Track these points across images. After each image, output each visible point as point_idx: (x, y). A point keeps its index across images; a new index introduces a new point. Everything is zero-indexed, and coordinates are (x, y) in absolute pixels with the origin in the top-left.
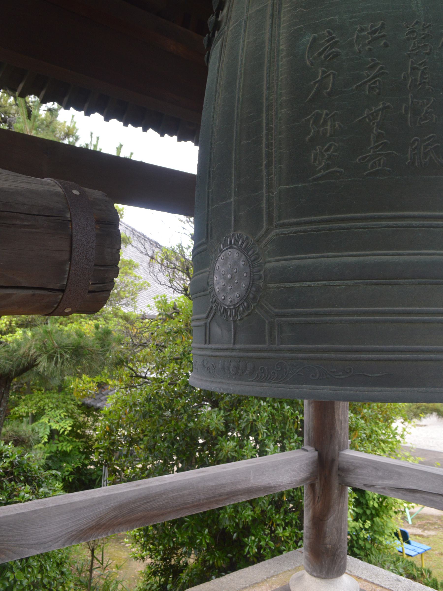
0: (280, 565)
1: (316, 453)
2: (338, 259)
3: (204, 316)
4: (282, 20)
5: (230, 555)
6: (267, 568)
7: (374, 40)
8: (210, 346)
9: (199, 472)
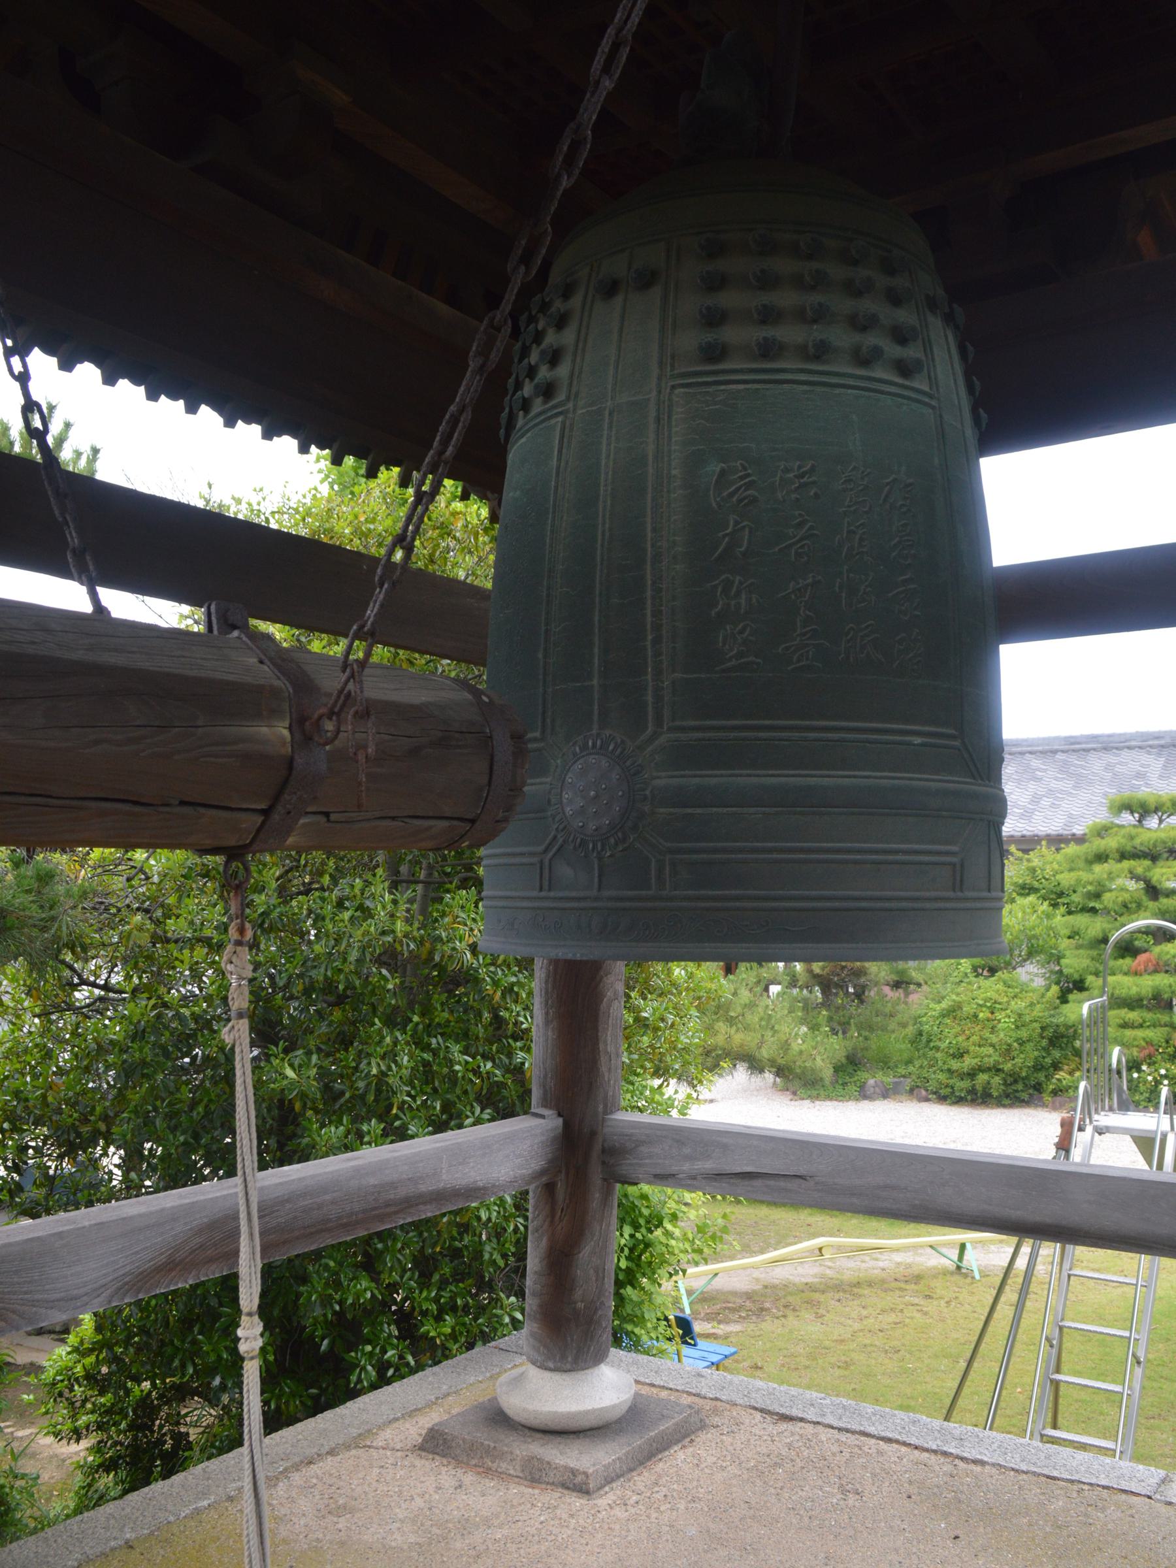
0: (459, 1374)
1: (560, 1121)
2: (754, 780)
3: (541, 848)
4: (674, 430)
5: (314, 1391)
6: (431, 1383)
7: (802, 486)
8: (552, 894)
9: (349, 1160)
